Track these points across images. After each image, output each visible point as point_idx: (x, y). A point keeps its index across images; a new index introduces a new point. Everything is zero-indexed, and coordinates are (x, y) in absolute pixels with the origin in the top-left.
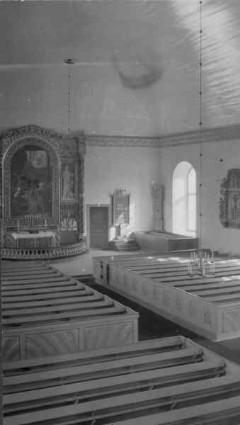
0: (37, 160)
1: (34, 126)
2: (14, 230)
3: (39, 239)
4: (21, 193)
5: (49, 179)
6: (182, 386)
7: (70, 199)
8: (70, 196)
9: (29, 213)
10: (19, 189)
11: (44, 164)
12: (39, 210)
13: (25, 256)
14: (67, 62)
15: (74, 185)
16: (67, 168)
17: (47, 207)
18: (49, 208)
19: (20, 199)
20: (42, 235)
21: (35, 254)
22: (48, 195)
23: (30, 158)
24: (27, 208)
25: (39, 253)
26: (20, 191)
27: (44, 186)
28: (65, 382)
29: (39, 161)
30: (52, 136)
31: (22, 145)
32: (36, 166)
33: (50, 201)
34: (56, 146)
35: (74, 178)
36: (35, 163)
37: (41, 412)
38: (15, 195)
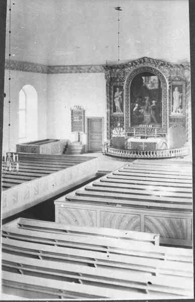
0: (151, 83)
1: (146, 58)
2: (131, 135)
3: (146, 143)
4: (139, 108)
5: (160, 99)
6: (134, 269)
7: (180, 114)
8: (179, 112)
9: (145, 123)
10: (137, 105)
11: (156, 86)
12: (152, 121)
13: (135, 155)
14: (116, 9)
15: (182, 103)
16: (176, 89)
17: (157, 119)
18: (159, 121)
19: (138, 113)
20: (149, 140)
21: (146, 154)
22: (158, 110)
23: (145, 82)
24: (143, 119)
25: (137, 154)
26: (138, 107)
27: (156, 103)
28: (59, 243)
29: (153, 84)
30: (162, 65)
31: (139, 72)
32: (150, 88)
33: (160, 115)
34: (166, 73)
35: (182, 97)
36: (149, 86)
37: (125, 279)
38: (134, 110)
